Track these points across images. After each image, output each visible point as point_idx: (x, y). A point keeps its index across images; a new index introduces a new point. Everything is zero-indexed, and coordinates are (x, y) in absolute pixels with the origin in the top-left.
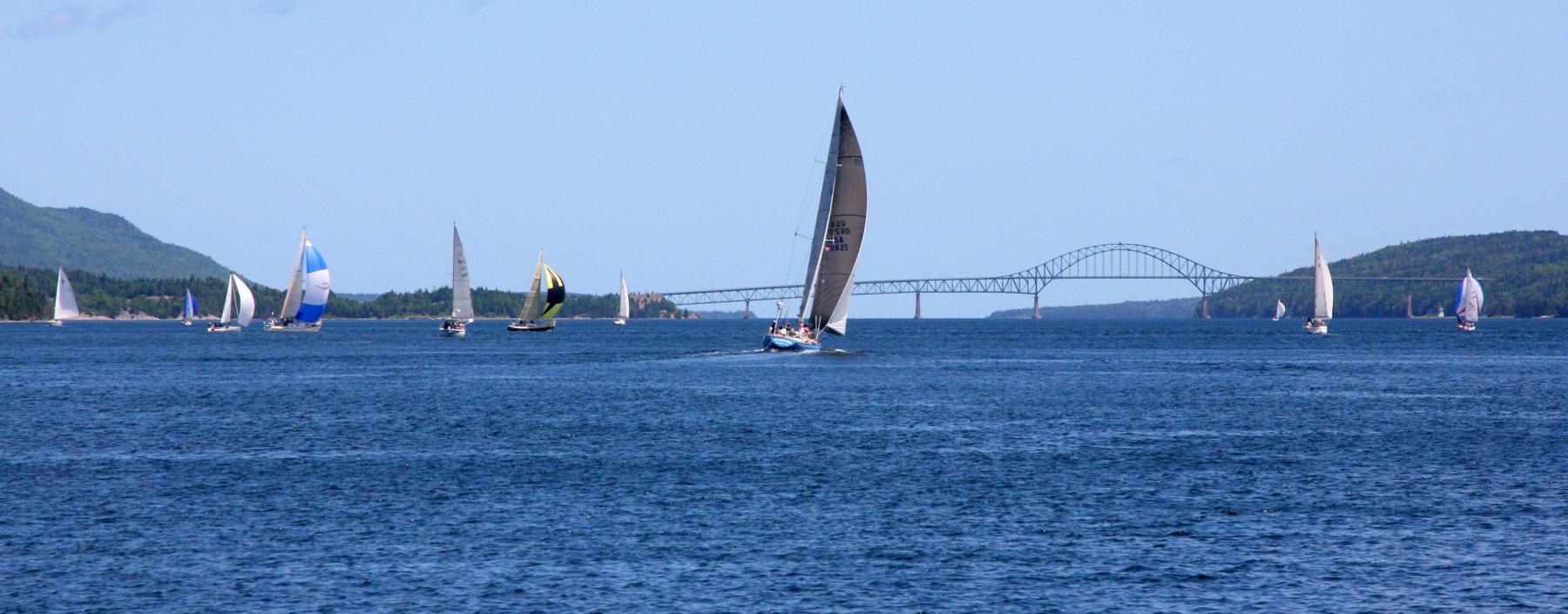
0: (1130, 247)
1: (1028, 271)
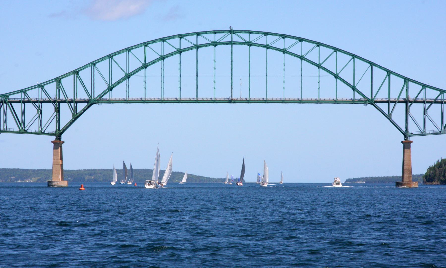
0: (253, 38)
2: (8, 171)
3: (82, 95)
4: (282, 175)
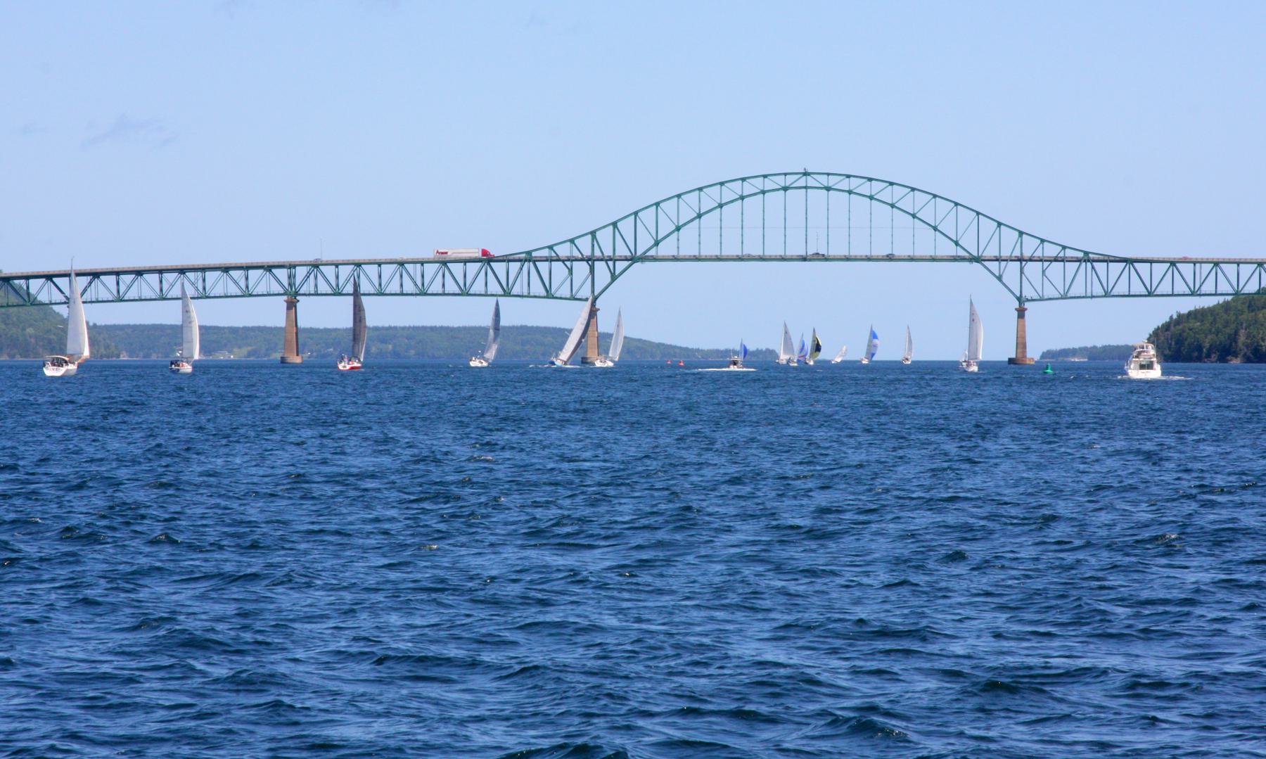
0: (832, 181)
1: (572, 241)
2: (169, 331)
3: (622, 251)
4: (910, 337)
